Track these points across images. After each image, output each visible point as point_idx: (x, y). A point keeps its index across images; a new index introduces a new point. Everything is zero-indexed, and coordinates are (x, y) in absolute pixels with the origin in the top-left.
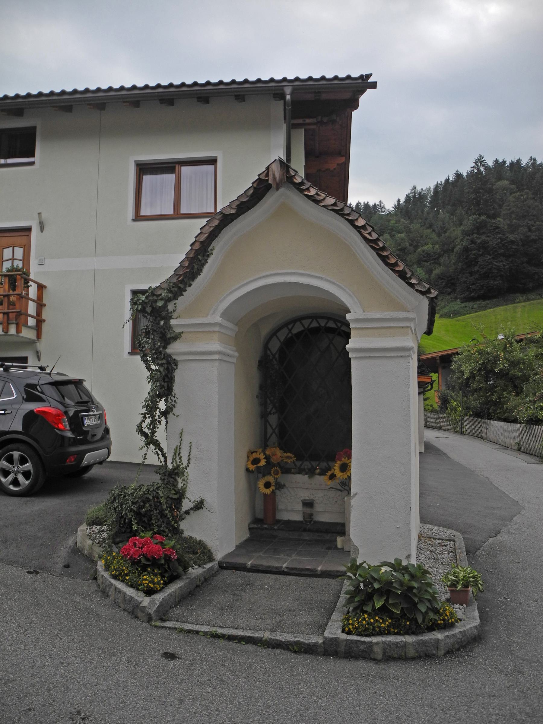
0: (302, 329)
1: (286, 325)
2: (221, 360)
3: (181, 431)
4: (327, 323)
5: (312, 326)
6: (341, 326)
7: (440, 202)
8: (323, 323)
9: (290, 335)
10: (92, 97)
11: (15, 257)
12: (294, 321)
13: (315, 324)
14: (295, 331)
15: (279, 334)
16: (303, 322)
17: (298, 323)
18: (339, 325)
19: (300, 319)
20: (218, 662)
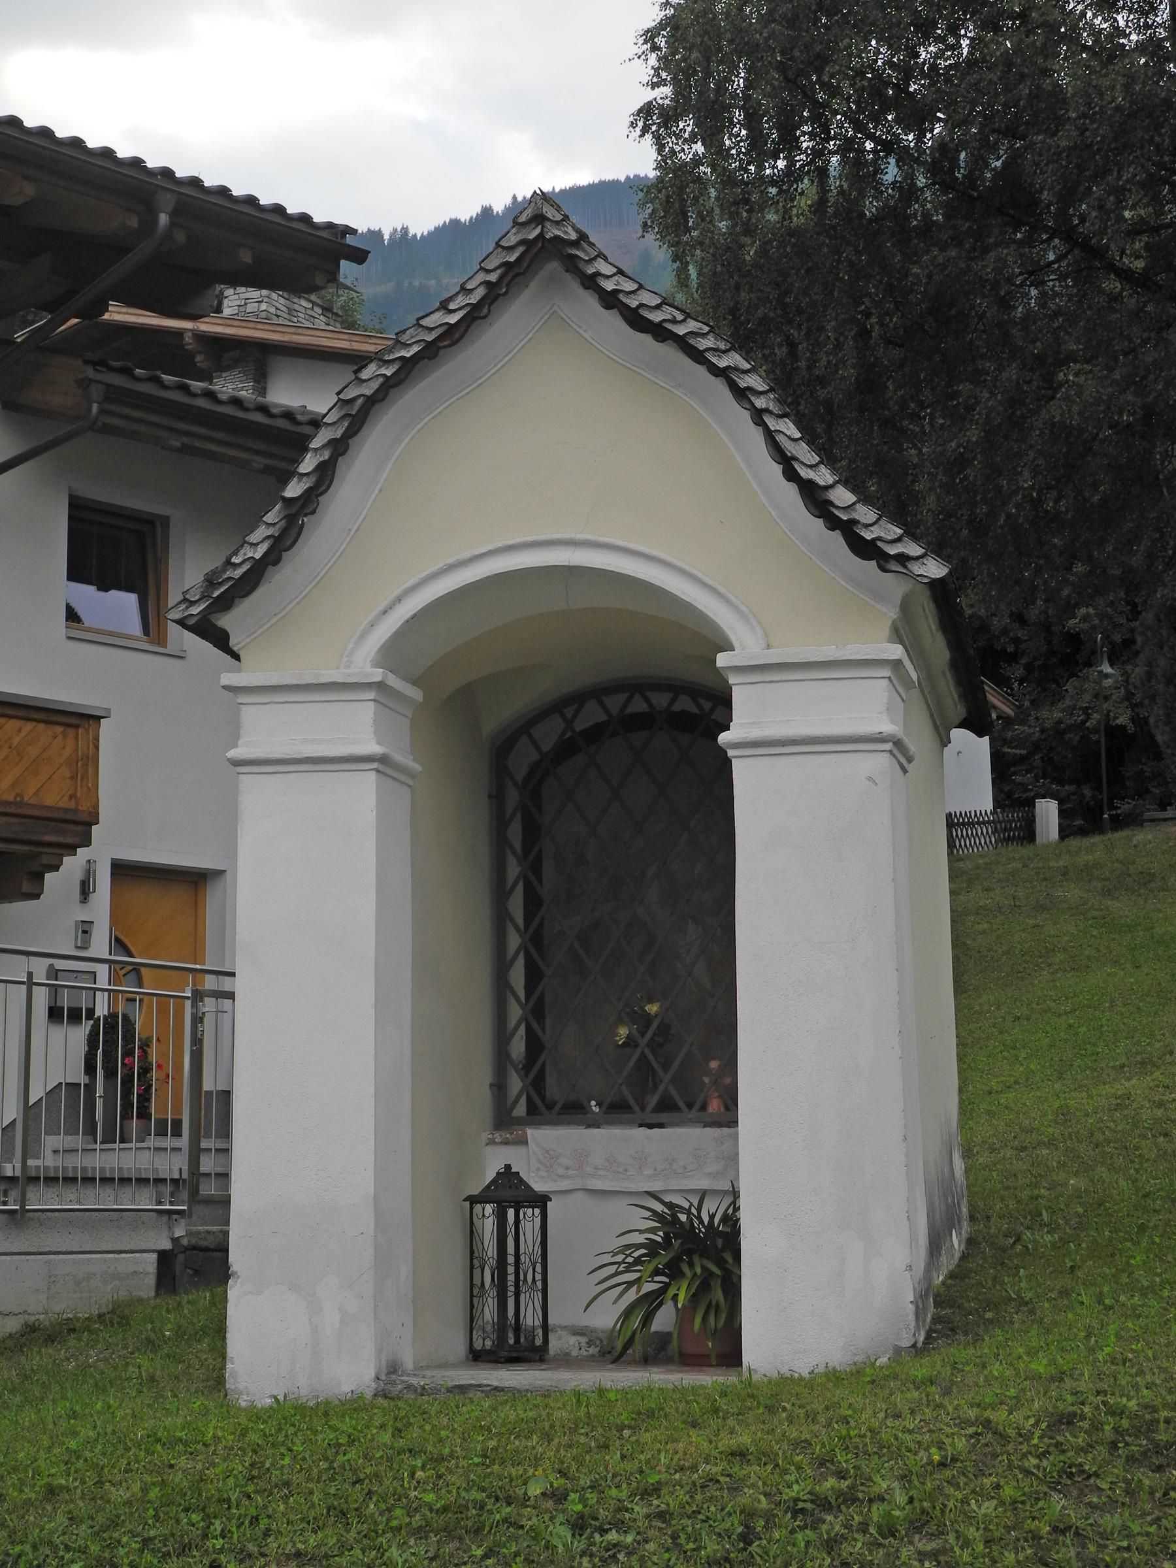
0: (603, 718)
1: (556, 707)
2: (379, 702)
3: (233, 642)
4: (673, 701)
5: (630, 710)
6: (713, 709)
7: (1027, 250)
8: (660, 700)
9: (569, 734)
10: (134, 178)
11: (24, 988)
12: (579, 698)
13: (638, 706)
14: (580, 725)
15: (536, 731)
16: (606, 700)
17: (592, 705)
18: (707, 705)
19: (597, 693)
20: (1128, 1549)
